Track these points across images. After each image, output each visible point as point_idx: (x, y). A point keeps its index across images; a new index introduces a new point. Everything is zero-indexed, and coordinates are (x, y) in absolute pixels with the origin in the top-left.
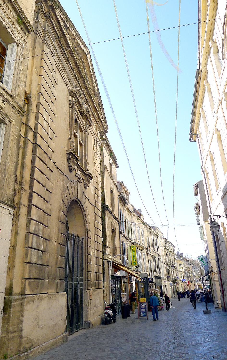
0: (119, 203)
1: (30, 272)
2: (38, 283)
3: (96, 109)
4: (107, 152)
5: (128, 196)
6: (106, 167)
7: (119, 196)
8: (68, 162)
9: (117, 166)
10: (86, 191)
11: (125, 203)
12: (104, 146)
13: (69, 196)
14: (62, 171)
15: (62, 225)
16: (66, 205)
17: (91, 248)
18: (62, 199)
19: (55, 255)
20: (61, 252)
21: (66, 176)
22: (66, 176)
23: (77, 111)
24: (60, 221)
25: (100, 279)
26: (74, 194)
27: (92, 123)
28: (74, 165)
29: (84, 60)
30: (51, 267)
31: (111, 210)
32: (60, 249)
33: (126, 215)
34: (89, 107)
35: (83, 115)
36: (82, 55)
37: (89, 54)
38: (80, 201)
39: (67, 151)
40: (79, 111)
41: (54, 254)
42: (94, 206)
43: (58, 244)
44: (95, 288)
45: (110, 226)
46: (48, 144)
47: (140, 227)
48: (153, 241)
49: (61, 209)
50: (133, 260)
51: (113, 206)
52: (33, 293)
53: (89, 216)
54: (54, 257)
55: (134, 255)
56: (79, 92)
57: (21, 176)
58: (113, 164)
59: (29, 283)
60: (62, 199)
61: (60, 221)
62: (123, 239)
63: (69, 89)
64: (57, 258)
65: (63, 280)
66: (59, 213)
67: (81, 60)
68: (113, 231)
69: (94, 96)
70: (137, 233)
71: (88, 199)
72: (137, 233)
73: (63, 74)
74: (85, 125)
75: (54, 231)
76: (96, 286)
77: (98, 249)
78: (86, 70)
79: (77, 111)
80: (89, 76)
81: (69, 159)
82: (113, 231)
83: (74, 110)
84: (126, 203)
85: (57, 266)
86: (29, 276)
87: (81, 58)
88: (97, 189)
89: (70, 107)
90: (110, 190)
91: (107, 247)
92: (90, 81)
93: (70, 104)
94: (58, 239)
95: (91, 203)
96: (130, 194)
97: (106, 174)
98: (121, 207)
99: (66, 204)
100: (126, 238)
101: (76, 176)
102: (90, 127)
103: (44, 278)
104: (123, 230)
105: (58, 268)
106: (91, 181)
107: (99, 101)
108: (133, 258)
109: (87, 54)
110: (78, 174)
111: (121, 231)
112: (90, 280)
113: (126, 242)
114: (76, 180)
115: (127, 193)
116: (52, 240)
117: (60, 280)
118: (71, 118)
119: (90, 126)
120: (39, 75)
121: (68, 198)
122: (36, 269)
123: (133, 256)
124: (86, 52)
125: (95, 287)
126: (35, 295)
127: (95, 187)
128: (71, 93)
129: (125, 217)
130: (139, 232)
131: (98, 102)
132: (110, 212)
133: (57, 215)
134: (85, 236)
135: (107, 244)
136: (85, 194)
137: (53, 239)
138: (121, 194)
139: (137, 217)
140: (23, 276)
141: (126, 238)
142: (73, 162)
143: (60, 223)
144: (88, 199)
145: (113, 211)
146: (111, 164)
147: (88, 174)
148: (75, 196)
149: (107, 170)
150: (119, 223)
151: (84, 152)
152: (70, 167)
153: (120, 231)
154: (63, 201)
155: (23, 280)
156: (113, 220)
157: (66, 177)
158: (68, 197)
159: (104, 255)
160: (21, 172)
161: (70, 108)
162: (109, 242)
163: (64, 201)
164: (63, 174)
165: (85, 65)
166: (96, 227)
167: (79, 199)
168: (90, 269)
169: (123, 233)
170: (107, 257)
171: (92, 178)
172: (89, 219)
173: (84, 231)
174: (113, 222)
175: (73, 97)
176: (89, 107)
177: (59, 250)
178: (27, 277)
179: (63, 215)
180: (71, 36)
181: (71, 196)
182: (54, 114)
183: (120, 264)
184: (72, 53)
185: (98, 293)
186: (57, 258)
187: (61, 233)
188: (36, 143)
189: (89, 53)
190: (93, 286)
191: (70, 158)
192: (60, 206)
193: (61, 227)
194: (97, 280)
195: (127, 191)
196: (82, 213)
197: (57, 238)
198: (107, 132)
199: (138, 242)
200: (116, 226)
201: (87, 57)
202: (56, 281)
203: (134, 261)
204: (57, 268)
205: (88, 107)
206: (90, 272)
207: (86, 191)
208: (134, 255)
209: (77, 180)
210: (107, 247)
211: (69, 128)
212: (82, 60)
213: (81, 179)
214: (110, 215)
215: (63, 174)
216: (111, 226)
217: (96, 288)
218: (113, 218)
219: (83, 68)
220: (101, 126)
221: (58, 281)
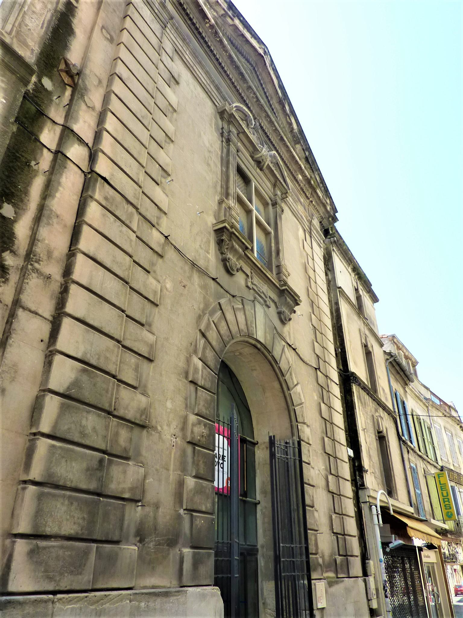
0: (390, 375)
1: (38, 513)
2: (86, 553)
3: (300, 165)
4: (343, 264)
5: (414, 366)
6: (342, 293)
7: (388, 359)
8: (219, 250)
9: (375, 299)
10: (286, 330)
11: (406, 379)
12: (333, 250)
13: (226, 327)
14: (201, 263)
15: (199, 393)
16: (215, 347)
17: (312, 470)
18: (200, 330)
19: (171, 472)
20: (198, 465)
21: (213, 279)
22: (213, 279)
23: (242, 152)
24: (191, 382)
25: (352, 551)
26: (242, 326)
27: (288, 187)
28: (238, 260)
29: (260, 70)
30: (157, 506)
31: (368, 387)
32: (193, 458)
33: (411, 404)
34: (276, 153)
35: (263, 165)
36: (253, 58)
37: (269, 56)
38: (265, 347)
39: (214, 225)
40: (252, 157)
41: (168, 470)
42: (316, 369)
43: (185, 444)
44: (337, 575)
45: (369, 421)
46: (140, 187)
47: (454, 433)
48: (267, 186)
49: (195, 352)
50: (445, 506)
51: (375, 381)
52: (51, 588)
53: (299, 388)
54: (168, 478)
55: (445, 494)
56: (246, 116)
57: (33, 237)
58: (364, 293)
59: (32, 553)
60: (200, 330)
61: (191, 382)
62: (413, 460)
63: (218, 105)
64: (181, 484)
65: (210, 549)
66: (188, 361)
67: (253, 70)
68: (381, 438)
69: (293, 143)
70: (447, 446)
71: (294, 349)
72: (447, 446)
73: (196, 70)
74: (272, 191)
75: (169, 405)
76: (339, 570)
77: (338, 473)
78: (267, 90)
79: (242, 152)
80: (275, 102)
81: (220, 243)
82: (381, 438)
83: (233, 149)
84: (409, 379)
85: (181, 506)
86: (36, 525)
87: (252, 66)
88: (322, 333)
89: (222, 141)
90: (360, 343)
91: (367, 471)
92: (280, 111)
93: (222, 134)
94: (183, 429)
95: (306, 359)
96: (417, 363)
97: (345, 309)
98: (397, 386)
99: (214, 343)
100: (420, 457)
101: (247, 287)
102: (287, 197)
103: (116, 538)
104: (410, 437)
105: (186, 512)
106: (296, 308)
107: (307, 153)
108: (444, 502)
109: (263, 55)
110: (255, 285)
111: (403, 438)
112: (316, 554)
113: (421, 466)
114: (253, 299)
115: (411, 360)
116: (159, 428)
117: (193, 547)
118: (225, 162)
119: (285, 194)
120: (115, 42)
121: (222, 332)
122: (73, 508)
123: (448, 499)
124: (261, 51)
125: (336, 572)
126: (59, 596)
127: (314, 328)
128: (222, 114)
129: (412, 410)
130: (452, 445)
131: (305, 154)
132: (364, 388)
133: (182, 364)
134: (293, 434)
135: (366, 463)
136: (284, 335)
137: (165, 427)
138: (392, 356)
139: (441, 412)
140: (11, 525)
141: (420, 457)
142: (232, 249)
143: (192, 387)
144: (294, 349)
145: (376, 391)
146: (357, 290)
147: (284, 288)
148: (246, 330)
149: (347, 299)
150: (393, 417)
151: (273, 245)
152: (225, 261)
153: (400, 438)
154: (204, 335)
155: (8, 542)
156: (376, 411)
157: (212, 281)
158: (220, 329)
159: (360, 492)
160: (35, 228)
161: (222, 143)
162: (370, 457)
163: (208, 334)
164: (203, 272)
165: (263, 79)
166: (325, 419)
167: (264, 343)
168: (313, 522)
169: (409, 443)
170: (368, 496)
171: (298, 299)
172: (300, 395)
173: (288, 425)
174: (377, 414)
175: (229, 122)
176: (277, 151)
177: (190, 460)
178: (23, 527)
179: (203, 368)
180: (215, 8)
181: (234, 329)
182: (166, 134)
183: (411, 514)
184: (216, 33)
185: (348, 590)
186: (181, 484)
187: (197, 415)
188: (92, 171)
189: (267, 52)
190: (331, 571)
191: (222, 240)
192: (193, 344)
193: (196, 398)
194: (341, 553)
195: (410, 356)
196: (278, 379)
197: (180, 426)
198: (335, 219)
199: (452, 468)
200: (387, 425)
201: (264, 61)
202: (174, 553)
203: (446, 509)
204: (182, 511)
205: (274, 152)
206: (317, 531)
207: (286, 330)
208: (445, 494)
209: (255, 298)
210: (367, 471)
211: (222, 182)
212: (254, 69)
213: (266, 297)
214: (367, 397)
215: (203, 272)
216: (371, 423)
217: (339, 576)
218: (377, 406)
219: (260, 86)
220: (318, 205)
221: (187, 551)
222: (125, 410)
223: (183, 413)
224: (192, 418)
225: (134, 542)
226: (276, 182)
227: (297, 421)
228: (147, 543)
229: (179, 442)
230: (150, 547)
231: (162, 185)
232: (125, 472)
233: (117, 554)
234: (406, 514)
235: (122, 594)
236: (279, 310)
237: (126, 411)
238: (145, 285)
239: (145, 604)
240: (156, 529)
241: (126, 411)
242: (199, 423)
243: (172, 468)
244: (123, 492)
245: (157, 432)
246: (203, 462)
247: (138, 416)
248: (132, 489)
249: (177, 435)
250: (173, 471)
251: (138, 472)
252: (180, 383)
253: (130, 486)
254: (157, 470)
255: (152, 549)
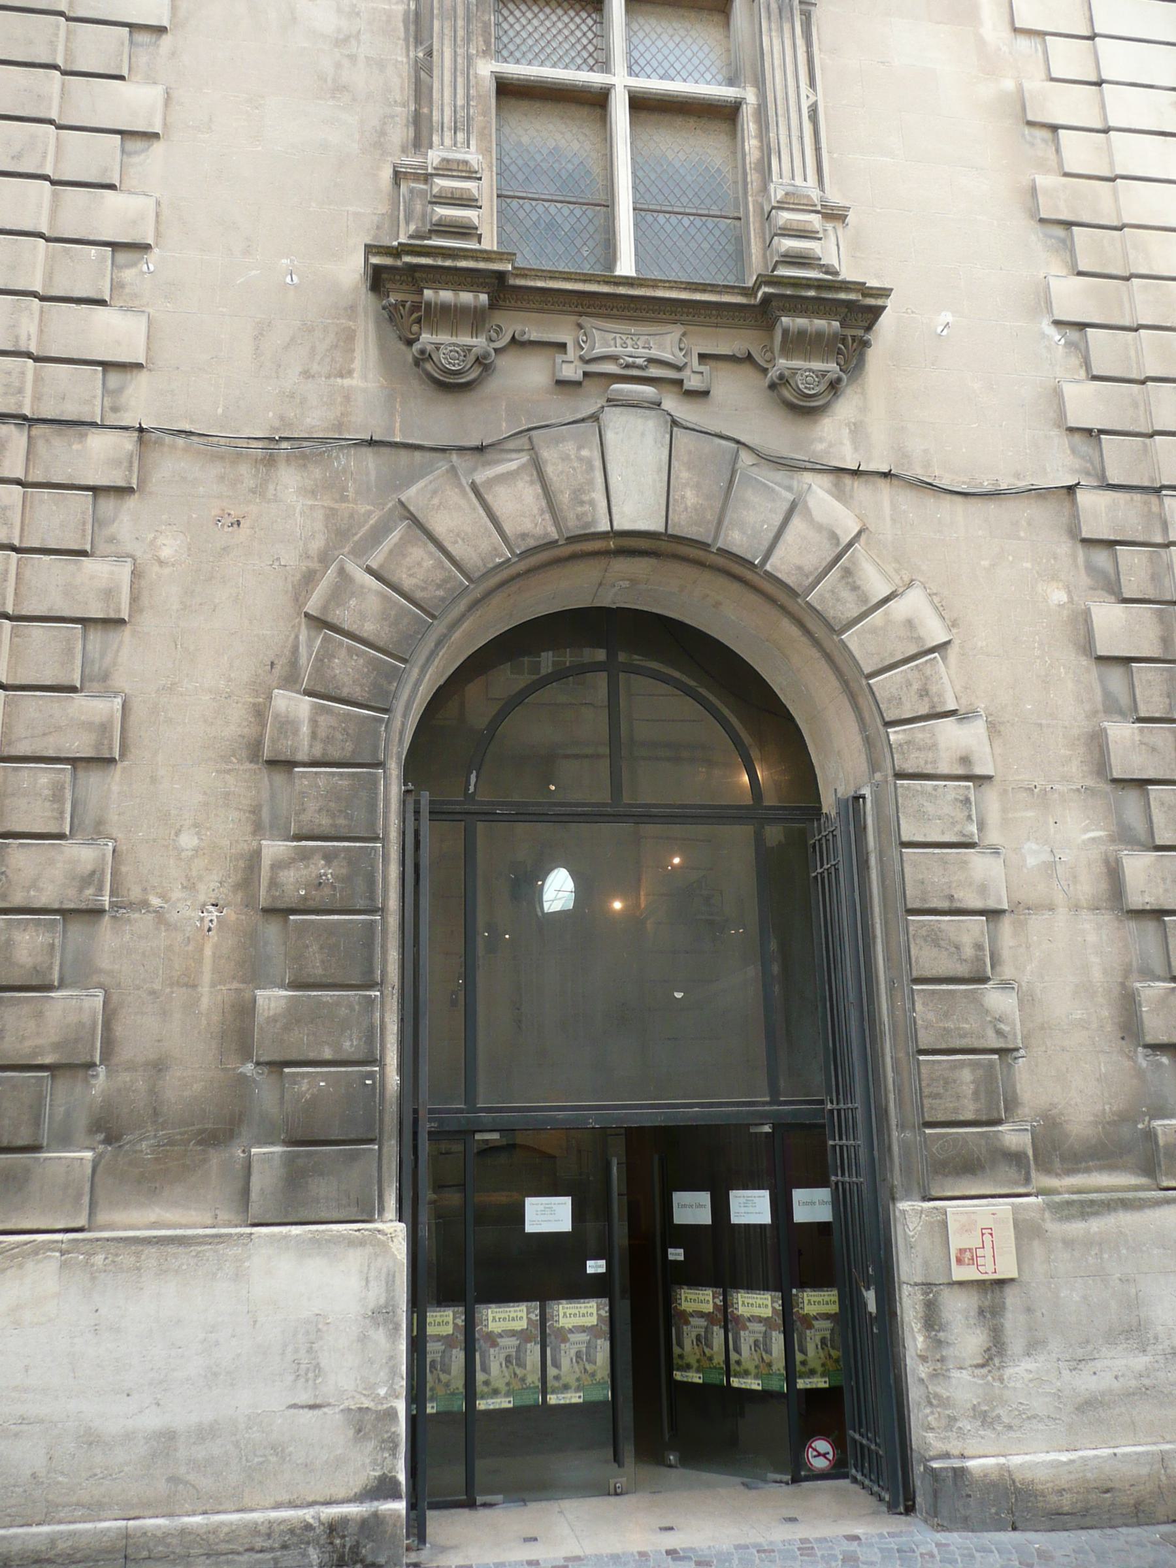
19: (205, 989)
30: (158, 1067)
137: (177, 894)
222: (28, 892)
223: (245, 845)
224: (274, 848)
225: (87, 1143)
226: (1164, 1439)
227: (831, 629)
228: (127, 1143)
229: (233, 917)
230: (141, 1151)
231: (1008, 972)
232: (39, 1015)
233: (27, 1170)
234: (7, 1153)
235: (34, 1241)
236: (773, 374)
237: (32, 893)
238: (68, 591)
239: (106, 1258)
240: (156, 1113)
241: (32, 893)
242: (304, 856)
243: (207, 977)
244: (35, 1054)
245: (148, 911)
246: (321, 948)
247: (72, 892)
248: (56, 1046)
249: (221, 903)
250: (213, 985)
251: (81, 1009)
252: (230, 779)
253: (55, 1039)
254: (153, 993)
255: (147, 1154)
